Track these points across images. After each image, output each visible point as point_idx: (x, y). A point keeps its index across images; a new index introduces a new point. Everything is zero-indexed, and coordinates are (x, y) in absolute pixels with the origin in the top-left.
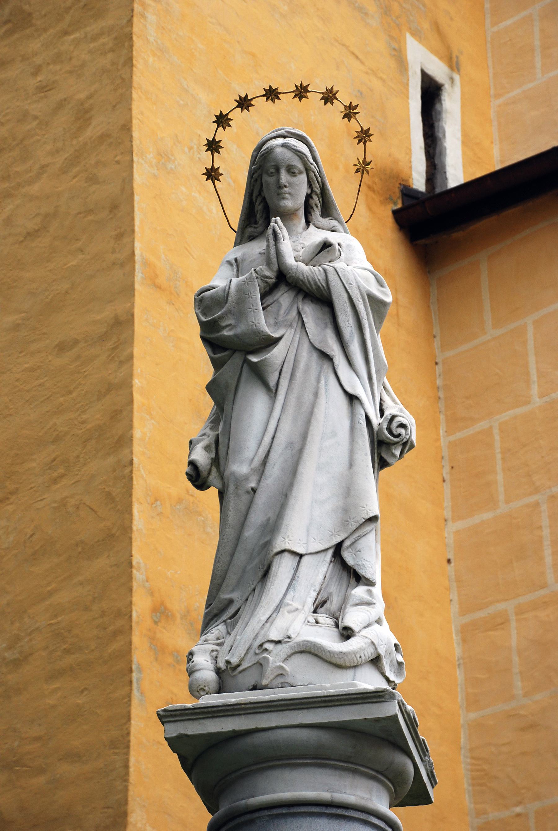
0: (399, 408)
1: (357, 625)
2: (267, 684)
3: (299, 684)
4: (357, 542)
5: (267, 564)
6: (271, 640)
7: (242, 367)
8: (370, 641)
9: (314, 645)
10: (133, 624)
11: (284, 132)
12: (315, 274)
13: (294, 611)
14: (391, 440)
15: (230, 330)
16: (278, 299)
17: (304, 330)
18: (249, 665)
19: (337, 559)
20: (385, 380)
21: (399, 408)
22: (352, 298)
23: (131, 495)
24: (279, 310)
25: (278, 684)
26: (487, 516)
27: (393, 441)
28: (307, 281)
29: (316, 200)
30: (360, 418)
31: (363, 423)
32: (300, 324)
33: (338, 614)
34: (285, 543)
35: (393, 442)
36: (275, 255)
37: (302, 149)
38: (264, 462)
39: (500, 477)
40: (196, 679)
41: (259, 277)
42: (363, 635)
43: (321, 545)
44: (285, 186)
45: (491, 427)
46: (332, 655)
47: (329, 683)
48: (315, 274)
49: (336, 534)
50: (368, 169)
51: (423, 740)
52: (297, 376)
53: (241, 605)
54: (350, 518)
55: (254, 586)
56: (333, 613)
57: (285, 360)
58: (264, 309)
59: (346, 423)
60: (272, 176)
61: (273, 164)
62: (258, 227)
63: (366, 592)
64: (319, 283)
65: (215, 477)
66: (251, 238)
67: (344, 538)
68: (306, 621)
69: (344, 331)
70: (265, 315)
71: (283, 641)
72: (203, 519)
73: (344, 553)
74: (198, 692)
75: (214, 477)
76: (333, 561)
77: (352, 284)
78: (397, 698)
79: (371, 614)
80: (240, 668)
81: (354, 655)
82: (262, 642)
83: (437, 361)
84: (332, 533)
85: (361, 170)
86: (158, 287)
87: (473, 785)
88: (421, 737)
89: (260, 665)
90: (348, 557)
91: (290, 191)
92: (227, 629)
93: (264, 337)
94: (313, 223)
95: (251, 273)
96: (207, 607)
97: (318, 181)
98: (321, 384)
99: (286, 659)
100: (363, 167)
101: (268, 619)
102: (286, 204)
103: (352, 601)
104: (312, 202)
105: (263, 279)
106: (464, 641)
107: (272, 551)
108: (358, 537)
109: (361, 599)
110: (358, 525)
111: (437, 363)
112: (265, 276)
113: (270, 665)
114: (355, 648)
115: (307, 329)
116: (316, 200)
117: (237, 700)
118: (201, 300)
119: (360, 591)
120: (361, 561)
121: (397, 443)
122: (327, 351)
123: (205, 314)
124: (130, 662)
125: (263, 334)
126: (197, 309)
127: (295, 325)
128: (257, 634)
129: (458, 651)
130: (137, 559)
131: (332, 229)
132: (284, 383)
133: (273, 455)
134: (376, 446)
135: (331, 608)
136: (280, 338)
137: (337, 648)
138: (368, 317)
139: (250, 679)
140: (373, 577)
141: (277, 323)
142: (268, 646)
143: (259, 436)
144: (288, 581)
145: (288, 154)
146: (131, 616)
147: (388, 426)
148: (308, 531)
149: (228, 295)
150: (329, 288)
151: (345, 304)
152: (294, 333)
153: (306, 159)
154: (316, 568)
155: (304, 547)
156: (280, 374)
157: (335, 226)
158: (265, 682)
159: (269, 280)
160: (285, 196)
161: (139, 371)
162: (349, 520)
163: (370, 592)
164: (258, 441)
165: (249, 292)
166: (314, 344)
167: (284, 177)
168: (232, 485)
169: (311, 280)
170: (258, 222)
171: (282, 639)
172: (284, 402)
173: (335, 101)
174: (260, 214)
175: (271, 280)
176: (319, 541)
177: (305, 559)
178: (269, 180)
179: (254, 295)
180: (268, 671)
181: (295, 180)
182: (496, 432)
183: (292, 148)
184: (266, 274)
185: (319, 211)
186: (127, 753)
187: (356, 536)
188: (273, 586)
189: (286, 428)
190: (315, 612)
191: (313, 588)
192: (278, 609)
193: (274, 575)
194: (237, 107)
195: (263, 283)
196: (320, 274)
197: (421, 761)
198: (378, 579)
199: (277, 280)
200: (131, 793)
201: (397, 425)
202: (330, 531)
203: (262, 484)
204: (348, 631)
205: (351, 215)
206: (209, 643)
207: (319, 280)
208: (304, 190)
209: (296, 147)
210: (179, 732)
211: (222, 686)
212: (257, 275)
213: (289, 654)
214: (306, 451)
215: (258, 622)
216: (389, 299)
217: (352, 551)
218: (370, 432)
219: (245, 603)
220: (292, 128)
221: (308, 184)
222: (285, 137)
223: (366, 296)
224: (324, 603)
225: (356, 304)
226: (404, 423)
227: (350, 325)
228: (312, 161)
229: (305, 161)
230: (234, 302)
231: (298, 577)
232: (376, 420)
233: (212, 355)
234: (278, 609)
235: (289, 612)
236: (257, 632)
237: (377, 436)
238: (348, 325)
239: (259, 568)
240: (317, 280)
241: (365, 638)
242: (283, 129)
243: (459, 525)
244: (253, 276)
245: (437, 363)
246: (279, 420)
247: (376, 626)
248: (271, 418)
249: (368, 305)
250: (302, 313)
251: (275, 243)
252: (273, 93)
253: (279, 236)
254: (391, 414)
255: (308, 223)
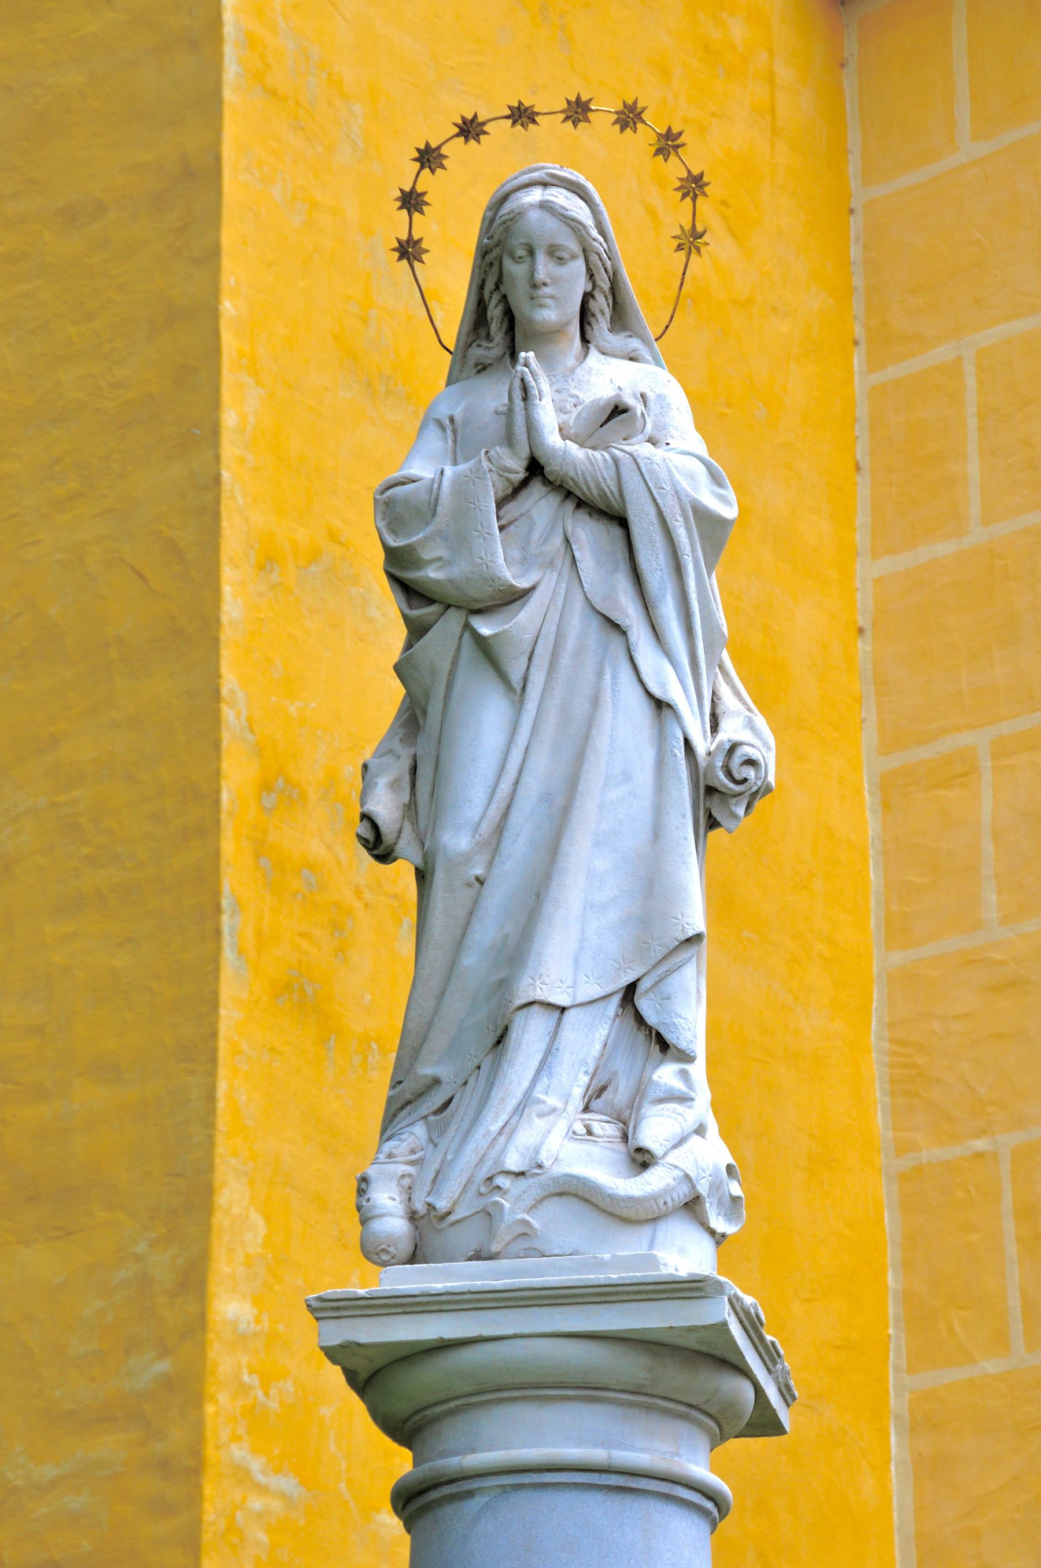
0: (745, 717)
1: (661, 1145)
2: (498, 1250)
3: (556, 1252)
4: (663, 981)
5: (502, 1026)
6: (507, 1170)
7: (461, 637)
8: (681, 1174)
9: (584, 1182)
10: (223, 817)
11: (545, 176)
12: (597, 468)
13: (549, 1113)
14: (730, 789)
15: (440, 568)
16: (528, 511)
17: (575, 574)
18: (468, 1213)
19: (628, 1011)
20: (725, 656)
21: (745, 717)
22: (665, 515)
23: (216, 549)
24: (529, 533)
25: (519, 1250)
26: (943, 549)
27: (733, 791)
28: (581, 481)
29: (601, 302)
30: (675, 744)
31: (679, 754)
32: (568, 562)
33: (627, 1113)
34: (535, 989)
35: (730, 792)
36: (524, 429)
37: (576, 213)
38: (500, 829)
39: (973, 469)
40: (373, 1233)
41: (494, 469)
42: (671, 1162)
43: (599, 988)
44: (545, 284)
45: (959, 358)
46: (615, 1202)
47: (610, 1253)
48: (597, 468)
49: (626, 966)
50: (699, 245)
51: (773, 1343)
52: (562, 665)
53: (454, 1092)
54: (652, 938)
55: (478, 1062)
56: (618, 1110)
57: (539, 632)
58: (501, 528)
59: (648, 754)
60: (518, 263)
61: (522, 240)
62: (492, 348)
63: (678, 1074)
64: (603, 485)
65: (409, 842)
66: (480, 367)
67: (641, 974)
68: (571, 1132)
69: (648, 579)
70: (504, 542)
71: (528, 1174)
72: (361, 590)
73: (640, 1001)
74: (377, 1254)
75: (407, 842)
76: (620, 1014)
77: (665, 487)
78: (727, 1292)
79: (686, 1121)
80: (452, 1218)
81: (653, 1202)
82: (492, 1172)
83: (852, 206)
84: (619, 963)
85: (686, 247)
86: (272, 93)
87: (892, 1094)
88: (769, 1338)
89: (489, 1215)
90: (645, 1005)
91: (554, 292)
92: (429, 1134)
93: (501, 588)
94: (596, 344)
95: (480, 461)
96: (392, 1085)
97: (605, 269)
98: (604, 682)
99: (534, 1207)
100: (689, 242)
101: (502, 1128)
102: (546, 317)
103: (653, 1094)
104: (592, 305)
105: (501, 474)
106: (886, 806)
107: (510, 1002)
108: (667, 971)
109: (668, 1091)
110: (667, 951)
111: (852, 211)
112: (506, 468)
113: (506, 1218)
114: (656, 1189)
115: (581, 573)
116: (601, 304)
117: (446, 1287)
118: (387, 503)
119: (666, 1074)
120: (671, 1017)
121: (740, 794)
122: (616, 618)
123: (394, 532)
124: (216, 893)
125: (500, 583)
126: (379, 518)
127: (559, 562)
128: (483, 1156)
129: (872, 825)
130: (230, 681)
131: (631, 355)
132: (537, 678)
133: (517, 818)
134: (702, 797)
135: (615, 1100)
136: (533, 588)
137: (624, 1189)
138: (693, 550)
139: (469, 1238)
140: (691, 1047)
141: (525, 559)
142: (502, 1181)
143: (491, 777)
144: (539, 1057)
145: (552, 224)
146: (217, 801)
147: (726, 762)
148: (576, 962)
149: (437, 500)
150: (621, 495)
151: (652, 528)
152: (557, 580)
153: (584, 232)
154: (590, 1029)
155: (568, 995)
156: (530, 660)
157: (635, 350)
158: (495, 1247)
159: (512, 476)
160: (543, 303)
161: (232, 282)
162: (650, 941)
163: (684, 1075)
164: (489, 787)
165: (476, 500)
166: (593, 603)
167: (544, 268)
168: (442, 871)
169: (589, 478)
170: (493, 338)
171: (528, 1169)
172: (537, 713)
173: (639, 125)
174: (497, 325)
175: (517, 475)
176: (596, 981)
177: (570, 1015)
178: (515, 270)
179: (484, 504)
180: (502, 1228)
181: (563, 271)
182: (969, 369)
183: (559, 213)
184: (507, 465)
185: (607, 322)
186: (213, 1073)
187: (661, 970)
188: (512, 1068)
189: (541, 763)
190: (586, 1109)
191: (583, 1069)
192: (521, 1109)
193: (514, 1047)
194: (457, 135)
195: (503, 481)
196: (607, 468)
197: (768, 1374)
198: (700, 1049)
199: (527, 474)
200: (219, 1150)
201: (741, 762)
202: (615, 962)
203: (495, 871)
204: (644, 1155)
205: (667, 327)
206: (396, 1162)
207: (604, 479)
208: (581, 285)
209: (567, 210)
210: (343, 1339)
211: (418, 1244)
212: (491, 466)
213: (539, 1198)
214: (576, 812)
215: (485, 1136)
216: (730, 512)
217: (654, 998)
218: (692, 768)
219: (462, 1089)
220: (559, 166)
221: (587, 275)
222: (545, 185)
223: (690, 510)
224: (603, 1089)
225: (671, 527)
226: (753, 758)
227: (659, 567)
228: (595, 233)
229: (582, 236)
230: (447, 516)
231: (558, 1049)
232: (701, 746)
233: (407, 611)
234: (521, 1109)
235: (540, 1116)
236: (482, 1152)
237: (705, 779)
238: (656, 567)
239: (488, 1029)
240: (601, 480)
241: (673, 1168)
242: (543, 168)
243: (887, 565)
244: (482, 467)
245: (852, 211)
246: (527, 749)
247: (696, 1138)
248: (513, 746)
249: (694, 528)
250: (572, 541)
251: (525, 405)
252: (524, 114)
253: (533, 393)
254: (729, 741)
255: (585, 340)
